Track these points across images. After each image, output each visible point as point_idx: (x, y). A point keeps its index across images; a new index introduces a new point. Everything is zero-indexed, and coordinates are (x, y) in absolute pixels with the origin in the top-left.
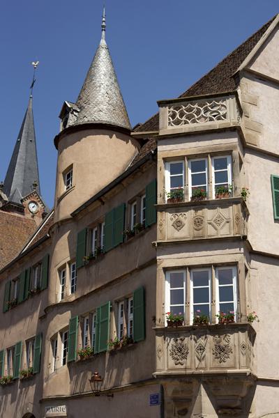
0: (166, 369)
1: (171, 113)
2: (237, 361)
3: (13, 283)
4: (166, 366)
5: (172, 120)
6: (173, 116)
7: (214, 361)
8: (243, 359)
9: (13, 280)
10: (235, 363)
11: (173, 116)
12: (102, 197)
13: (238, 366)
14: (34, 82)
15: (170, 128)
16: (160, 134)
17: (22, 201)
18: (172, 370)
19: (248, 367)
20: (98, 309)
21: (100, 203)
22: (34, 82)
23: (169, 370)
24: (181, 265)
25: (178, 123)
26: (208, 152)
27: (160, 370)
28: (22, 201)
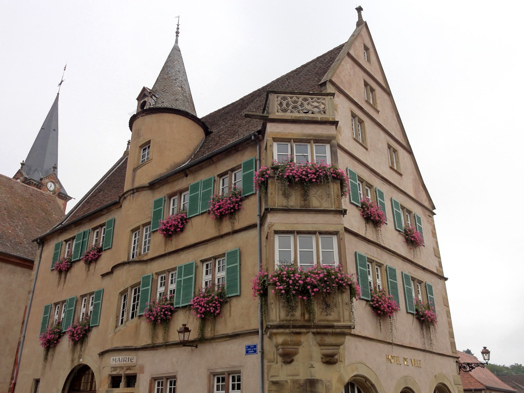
0: (278, 320)
1: (279, 102)
2: (341, 315)
3: (64, 243)
4: (278, 317)
5: (279, 108)
6: (281, 104)
7: (321, 314)
8: (347, 313)
9: (65, 241)
10: (340, 317)
11: (281, 104)
12: (187, 170)
13: (342, 320)
14: (62, 81)
15: (277, 114)
16: (269, 117)
17: (41, 179)
18: (283, 321)
19: (351, 321)
20: (180, 268)
21: (184, 175)
22: (62, 81)
23: (280, 321)
24: (290, 229)
25: (285, 111)
26: (311, 138)
27: (273, 321)
28: (41, 179)
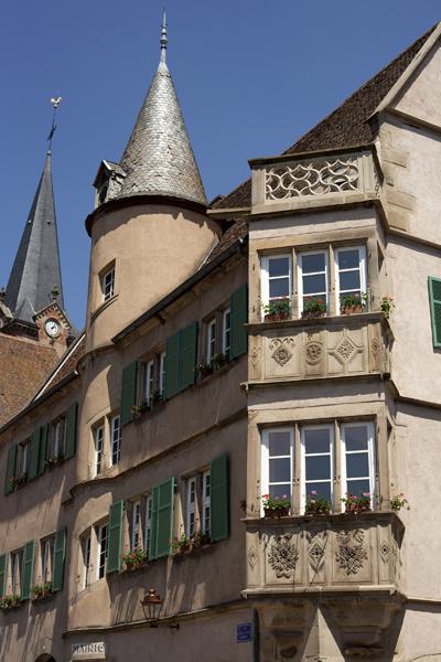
0: (263, 584)
1: (270, 179)
2: (375, 571)
3: (20, 448)
4: (262, 579)
5: (271, 190)
6: (274, 184)
7: (338, 571)
8: (384, 569)
9: (21, 444)
10: (372, 575)
11: (274, 184)
12: (161, 313)
13: (376, 579)
14: (54, 129)
15: (268, 202)
16: (253, 213)
17: (34, 318)
18: (271, 585)
19: (392, 582)
20: (156, 489)
21: (158, 322)
22: (54, 129)
23: (267, 585)
24: (286, 419)
25: (281, 194)
26: (329, 240)
27: (254, 586)
28: (34, 318)
